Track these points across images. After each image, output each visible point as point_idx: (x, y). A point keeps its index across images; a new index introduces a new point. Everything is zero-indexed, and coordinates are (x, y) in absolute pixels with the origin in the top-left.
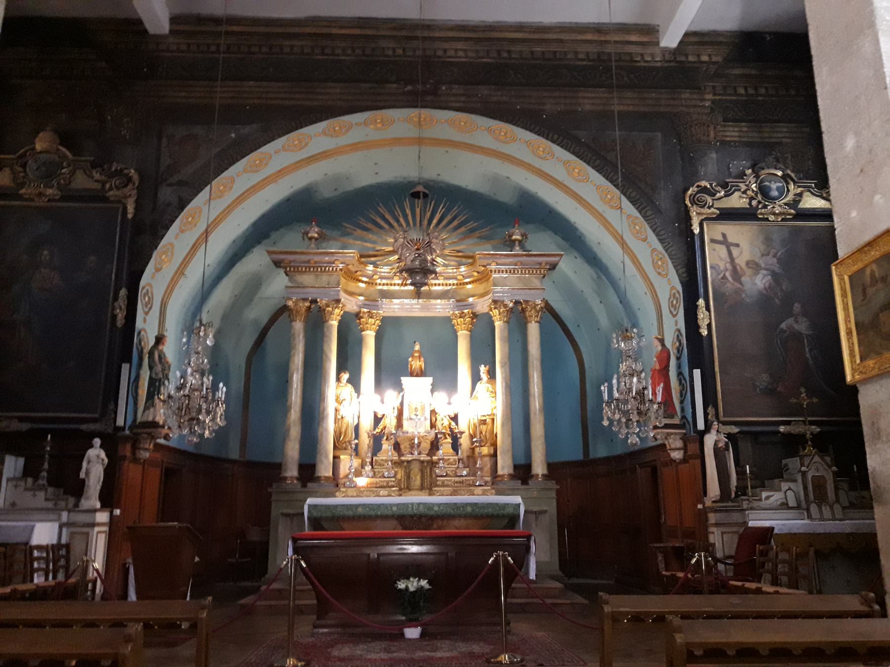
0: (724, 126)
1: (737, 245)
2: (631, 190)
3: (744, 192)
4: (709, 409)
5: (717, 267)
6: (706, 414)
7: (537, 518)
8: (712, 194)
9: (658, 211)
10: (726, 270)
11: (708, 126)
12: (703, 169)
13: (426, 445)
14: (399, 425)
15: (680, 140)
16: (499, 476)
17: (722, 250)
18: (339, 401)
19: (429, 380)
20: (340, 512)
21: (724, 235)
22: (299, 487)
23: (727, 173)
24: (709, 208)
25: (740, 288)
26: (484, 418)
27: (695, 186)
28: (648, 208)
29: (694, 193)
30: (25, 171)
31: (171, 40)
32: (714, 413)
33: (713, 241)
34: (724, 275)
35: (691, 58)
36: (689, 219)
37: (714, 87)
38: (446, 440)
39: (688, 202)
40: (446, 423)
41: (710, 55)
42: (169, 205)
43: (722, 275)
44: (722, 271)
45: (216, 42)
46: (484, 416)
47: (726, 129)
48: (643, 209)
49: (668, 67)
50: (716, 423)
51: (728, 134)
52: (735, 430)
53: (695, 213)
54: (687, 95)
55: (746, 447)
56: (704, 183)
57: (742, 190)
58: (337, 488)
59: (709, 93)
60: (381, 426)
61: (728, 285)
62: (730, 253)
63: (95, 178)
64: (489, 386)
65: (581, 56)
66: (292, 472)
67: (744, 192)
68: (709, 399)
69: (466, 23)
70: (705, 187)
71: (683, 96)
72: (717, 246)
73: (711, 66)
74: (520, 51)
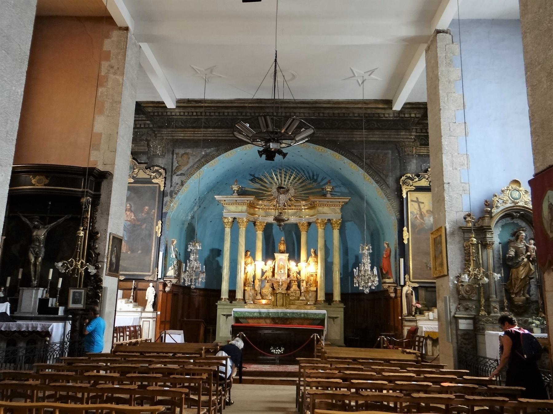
0: (421, 147)
1: (423, 203)
2: (376, 177)
3: (427, 179)
6: (405, 278)
9: (388, 186)
10: (417, 214)
11: (413, 148)
12: (409, 168)
13: (285, 286)
14: (273, 275)
15: (399, 154)
16: (318, 301)
17: (416, 205)
18: (246, 264)
19: (287, 255)
21: (417, 198)
23: (420, 170)
24: (411, 186)
26: (312, 274)
28: (383, 185)
31: (177, 111)
33: (412, 201)
35: (406, 116)
37: (416, 129)
39: (401, 183)
40: (295, 275)
41: (415, 114)
42: (177, 184)
43: (415, 217)
45: (196, 111)
47: (421, 149)
48: (381, 186)
49: (396, 119)
51: (422, 151)
52: (416, 285)
54: (404, 133)
55: (422, 293)
59: (414, 132)
60: (265, 276)
61: (418, 221)
62: (419, 206)
64: (315, 259)
65: (356, 115)
67: (427, 179)
68: (406, 272)
69: (304, 101)
71: (402, 134)
72: (413, 203)
73: (416, 119)
74: (328, 113)
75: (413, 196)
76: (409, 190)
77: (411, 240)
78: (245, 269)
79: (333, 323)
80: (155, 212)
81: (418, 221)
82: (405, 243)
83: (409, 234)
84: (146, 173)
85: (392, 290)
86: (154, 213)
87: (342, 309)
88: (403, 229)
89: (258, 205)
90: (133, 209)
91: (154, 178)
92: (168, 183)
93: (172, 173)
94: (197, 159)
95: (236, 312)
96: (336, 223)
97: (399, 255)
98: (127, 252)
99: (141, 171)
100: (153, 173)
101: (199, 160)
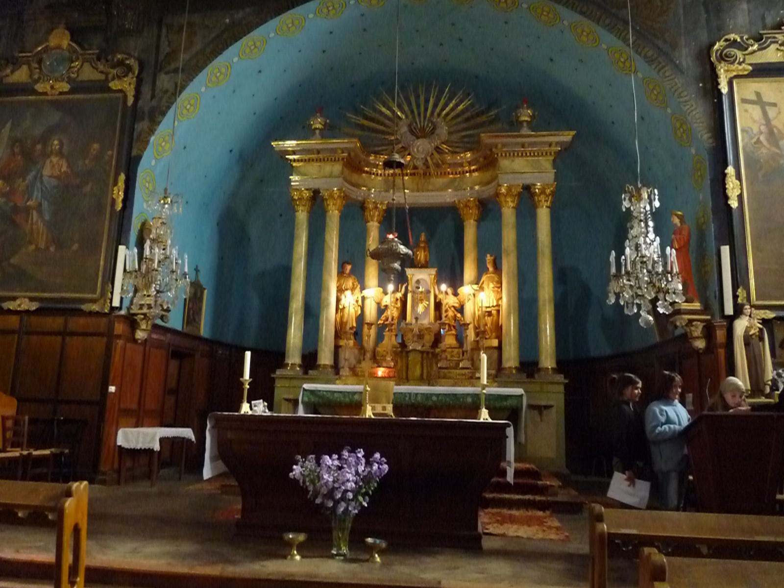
1: (775, 105)
4: (739, 290)
5: (749, 130)
6: (735, 297)
7: (541, 414)
8: (743, 47)
10: (761, 133)
12: (732, 22)
17: (755, 111)
18: (340, 290)
19: (433, 271)
20: (337, 398)
21: (758, 94)
22: (301, 374)
24: (740, 63)
25: (777, 153)
26: (489, 310)
27: (723, 39)
28: (666, 68)
29: (721, 48)
30: (40, 69)
32: (745, 295)
33: (744, 101)
34: (759, 139)
36: (715, 77)
38: (450, 332)
39: (713, 59)
42: (166, 91)
43: (755, 140)
44: (755, 135)
46: (489, 307)
50: (748, 307)
52: (770, 315)
53: (722, 70)
56: (732, 36)
57: (780, 42)
58: (337, 377)
60: (383, 317)
62: (765, 114)
63: (99, 70)
66: (294, 358)
68: (739, 280)
70: (735, 41)
72: (749, 107)
75: (746, 90)
76: (735, 73)
77: (748, 202)
78: (338, 300)
79: (539, 420)
80: (112, 154)
81: (764, 151)
82: (733, 206)
83: (741, 185)
84: (97, 69)
85: (697, 330)
86: (112, 156)
87: (561, 388)
88: (726, 171)
89: (368, 164)
90: (66, 149)
91: (113, 79)
92: (146, 90)
93: (156, 68)
94: (213, 35)
95: (312, 392)
96: (543, 192)
97: (716, 238)
98: (47, 248)
99: (87, 66)
100: (113, 67)
101: (218, 36)
